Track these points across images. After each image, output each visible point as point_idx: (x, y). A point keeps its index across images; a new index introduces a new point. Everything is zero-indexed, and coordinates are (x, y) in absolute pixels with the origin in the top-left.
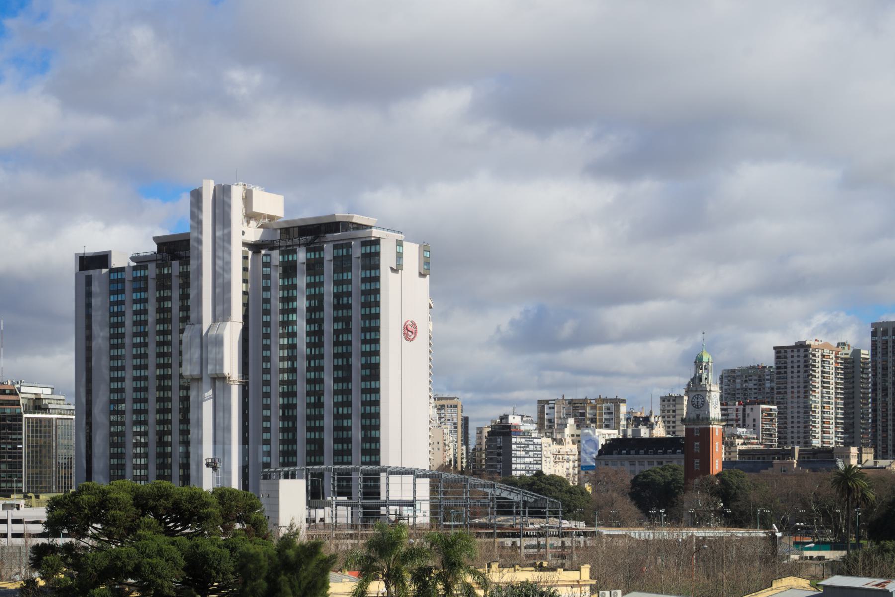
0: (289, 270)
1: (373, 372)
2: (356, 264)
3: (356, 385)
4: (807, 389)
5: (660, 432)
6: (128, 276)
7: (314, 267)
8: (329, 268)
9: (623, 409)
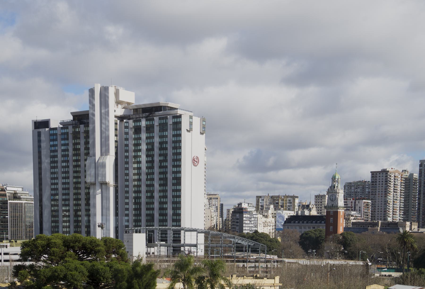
0: (138, 130)
1: (178, 181)
2: (170, 127)
4: (386, 193)
5: (314, 212)
6: (59, 132)
7: (150, 129)
8: (156, 129)
9: (297, 201)
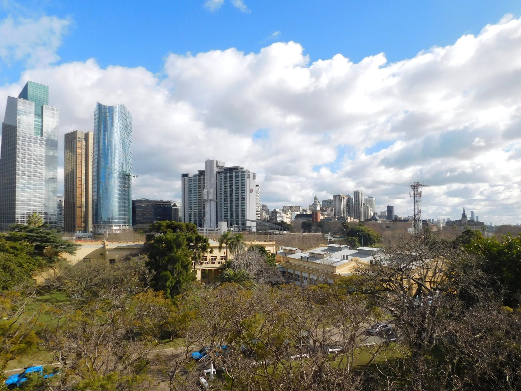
0: (226, 178)
1: (244, 199)
2: (240, 177)
3: (240, 202)
4: (340, 204)
5: (309, 213)
6: (193, 178)
7: (231, 177)
8: (234, 177)
9: (301, 208)
